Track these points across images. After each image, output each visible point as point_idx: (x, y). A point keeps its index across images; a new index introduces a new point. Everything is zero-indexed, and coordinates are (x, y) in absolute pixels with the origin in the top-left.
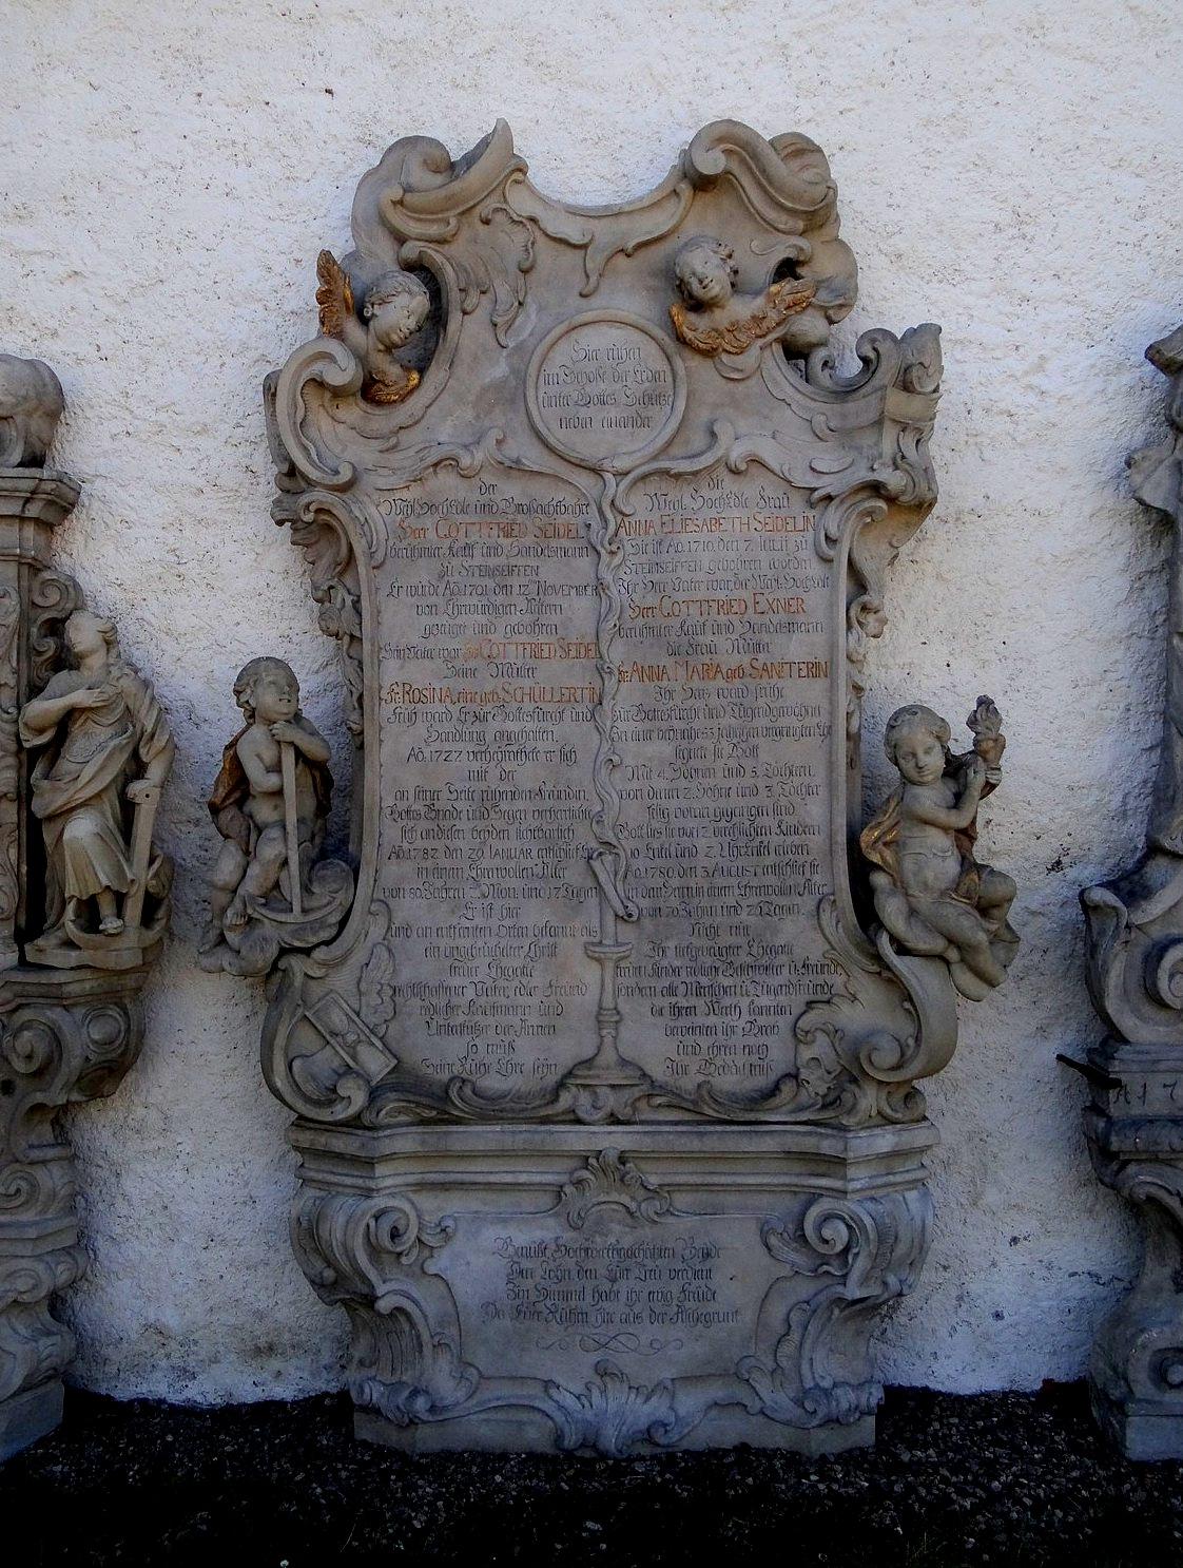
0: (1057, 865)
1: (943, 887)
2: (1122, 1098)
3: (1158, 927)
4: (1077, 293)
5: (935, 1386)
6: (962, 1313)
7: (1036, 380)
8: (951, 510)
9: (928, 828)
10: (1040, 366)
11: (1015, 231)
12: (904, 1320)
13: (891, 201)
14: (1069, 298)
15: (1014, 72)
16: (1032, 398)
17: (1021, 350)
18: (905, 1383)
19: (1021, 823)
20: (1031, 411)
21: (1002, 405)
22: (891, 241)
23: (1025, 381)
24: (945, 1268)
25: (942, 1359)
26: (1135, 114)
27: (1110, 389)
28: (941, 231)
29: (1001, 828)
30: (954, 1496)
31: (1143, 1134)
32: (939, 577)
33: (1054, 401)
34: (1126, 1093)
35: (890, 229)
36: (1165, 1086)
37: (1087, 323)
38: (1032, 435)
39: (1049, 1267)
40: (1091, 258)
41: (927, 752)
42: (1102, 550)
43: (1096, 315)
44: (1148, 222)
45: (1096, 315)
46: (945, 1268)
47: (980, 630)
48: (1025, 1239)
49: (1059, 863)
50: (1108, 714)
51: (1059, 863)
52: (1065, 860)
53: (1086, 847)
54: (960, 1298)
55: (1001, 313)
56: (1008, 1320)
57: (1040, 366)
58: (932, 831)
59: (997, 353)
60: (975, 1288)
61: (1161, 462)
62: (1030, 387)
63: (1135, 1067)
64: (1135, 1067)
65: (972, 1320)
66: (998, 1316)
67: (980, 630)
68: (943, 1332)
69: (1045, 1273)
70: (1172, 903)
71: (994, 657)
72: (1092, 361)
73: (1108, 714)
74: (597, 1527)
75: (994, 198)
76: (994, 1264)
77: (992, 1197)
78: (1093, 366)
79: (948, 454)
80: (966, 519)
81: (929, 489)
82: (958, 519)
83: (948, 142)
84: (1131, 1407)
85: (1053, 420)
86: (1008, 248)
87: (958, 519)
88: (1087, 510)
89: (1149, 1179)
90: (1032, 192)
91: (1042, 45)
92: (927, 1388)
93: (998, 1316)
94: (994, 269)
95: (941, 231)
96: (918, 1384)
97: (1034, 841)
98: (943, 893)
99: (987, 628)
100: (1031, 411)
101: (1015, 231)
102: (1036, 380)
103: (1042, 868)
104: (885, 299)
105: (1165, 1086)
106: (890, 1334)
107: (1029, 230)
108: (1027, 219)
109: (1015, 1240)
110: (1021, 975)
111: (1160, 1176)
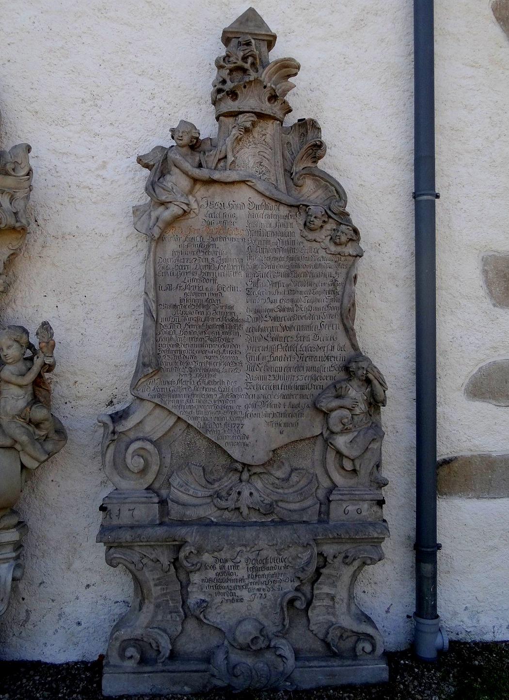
0: (111, 403)
1: (15, 413)
2: (108, 516)
3: (133, 433)
4: (121, 132)
5: (43, 659)
6: (61, 623)
7: (100, 173)
8: (60, 233)
9: (10, 385)
10: (104, 166)
11: (92, 103)
12: (30, 627)
13: (33, 87)
14: (119, 135)
15: (92, 29)
16: (100, 181)
17: (95, 158)
18: (29, 658)
19: (92, 383)
20: (99, 187)
21: (85, 184)
22: (32, 105)
23: (97, 173)
24: (53, 601)
25: (49, 647)
26: (150, 51)
27: (136, 179)
28: (56, 102)
29: (82, 385)
30: (451, 675)
31: (113, 534)
32: (53, 264)
33: (109, 183)
34: (110, 514)
35: (31, 100)
36: (129, 510)
37: (126, 147)
38: (99, 198)
39: (105, 599)
40: (128, 116)
41: (9, 347)
42: (133, 253)
43: (130, 143)
44: (155, 101)
45: (130, 143)
46: (53, 601)
47: (73, 290)
48: (93, 585)
49: (112, 402)
50: (134, 331)
51: (112, 402)
52: (115, 401)
53: (125, 394)
54: (60, 615)
55: (85, 141)
56: (83, 625)
57: (104, 166)
58: (12, 386)
59: (83, 160)
60: (67, 610)
61: (145, 212)
62: (99, 176)
63: (115, 501)
64: (115, 501)
65: (66, 626)
66: (79, 624)
67: (73, 290)
68: (51, 632)
69: (103, 602)
70: (138, 421)
71: (79, 303)
72: (127, 165)
73: (134, 331)
74: (473, 678)
75: (82, 87)
76: (77, 598)
77: (77, 564)
78: (128, 167)
79: (59, 207)
80: (67, 237)
81: (17, 221)
82: (63, 237)
83: (60, 60)
84: (106, 669)
85: (108, 192)
86: (89, 110)
87: (63, 237)
88: (125, 234)
89: (118, 556)
90: (99, 84)
91: (106, 17)
92: (40, 661)
93: (79, 624)
94: (82, 120)
95: (56, 102)
96: (36, 659)
97: (99, 391)
98: (14, 417)
99: (76, 289)
100: (99, 187)
101: (92, 103)
102: (100, 173)
103: (104, 404)
104: (29, 132)
105: (129, 510)
106: (23, 634)
107: (99, 103)
108: (98, 98)
109: (88, 586)
110: (94, 456)
111: (124, 554)
